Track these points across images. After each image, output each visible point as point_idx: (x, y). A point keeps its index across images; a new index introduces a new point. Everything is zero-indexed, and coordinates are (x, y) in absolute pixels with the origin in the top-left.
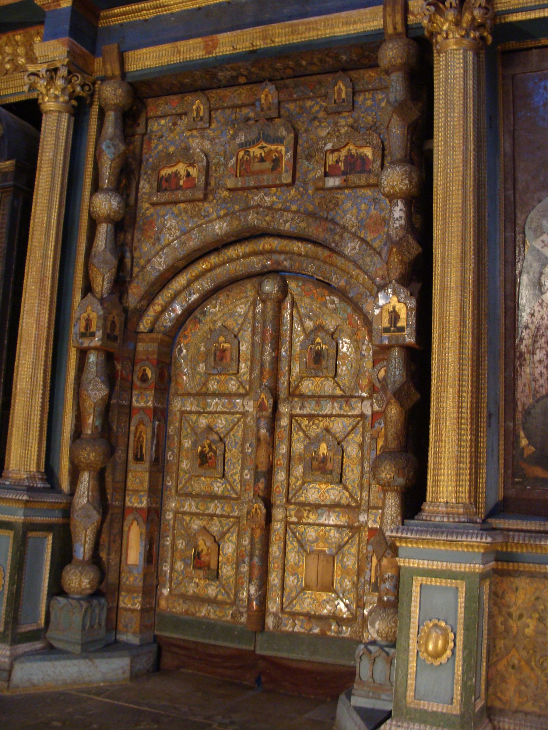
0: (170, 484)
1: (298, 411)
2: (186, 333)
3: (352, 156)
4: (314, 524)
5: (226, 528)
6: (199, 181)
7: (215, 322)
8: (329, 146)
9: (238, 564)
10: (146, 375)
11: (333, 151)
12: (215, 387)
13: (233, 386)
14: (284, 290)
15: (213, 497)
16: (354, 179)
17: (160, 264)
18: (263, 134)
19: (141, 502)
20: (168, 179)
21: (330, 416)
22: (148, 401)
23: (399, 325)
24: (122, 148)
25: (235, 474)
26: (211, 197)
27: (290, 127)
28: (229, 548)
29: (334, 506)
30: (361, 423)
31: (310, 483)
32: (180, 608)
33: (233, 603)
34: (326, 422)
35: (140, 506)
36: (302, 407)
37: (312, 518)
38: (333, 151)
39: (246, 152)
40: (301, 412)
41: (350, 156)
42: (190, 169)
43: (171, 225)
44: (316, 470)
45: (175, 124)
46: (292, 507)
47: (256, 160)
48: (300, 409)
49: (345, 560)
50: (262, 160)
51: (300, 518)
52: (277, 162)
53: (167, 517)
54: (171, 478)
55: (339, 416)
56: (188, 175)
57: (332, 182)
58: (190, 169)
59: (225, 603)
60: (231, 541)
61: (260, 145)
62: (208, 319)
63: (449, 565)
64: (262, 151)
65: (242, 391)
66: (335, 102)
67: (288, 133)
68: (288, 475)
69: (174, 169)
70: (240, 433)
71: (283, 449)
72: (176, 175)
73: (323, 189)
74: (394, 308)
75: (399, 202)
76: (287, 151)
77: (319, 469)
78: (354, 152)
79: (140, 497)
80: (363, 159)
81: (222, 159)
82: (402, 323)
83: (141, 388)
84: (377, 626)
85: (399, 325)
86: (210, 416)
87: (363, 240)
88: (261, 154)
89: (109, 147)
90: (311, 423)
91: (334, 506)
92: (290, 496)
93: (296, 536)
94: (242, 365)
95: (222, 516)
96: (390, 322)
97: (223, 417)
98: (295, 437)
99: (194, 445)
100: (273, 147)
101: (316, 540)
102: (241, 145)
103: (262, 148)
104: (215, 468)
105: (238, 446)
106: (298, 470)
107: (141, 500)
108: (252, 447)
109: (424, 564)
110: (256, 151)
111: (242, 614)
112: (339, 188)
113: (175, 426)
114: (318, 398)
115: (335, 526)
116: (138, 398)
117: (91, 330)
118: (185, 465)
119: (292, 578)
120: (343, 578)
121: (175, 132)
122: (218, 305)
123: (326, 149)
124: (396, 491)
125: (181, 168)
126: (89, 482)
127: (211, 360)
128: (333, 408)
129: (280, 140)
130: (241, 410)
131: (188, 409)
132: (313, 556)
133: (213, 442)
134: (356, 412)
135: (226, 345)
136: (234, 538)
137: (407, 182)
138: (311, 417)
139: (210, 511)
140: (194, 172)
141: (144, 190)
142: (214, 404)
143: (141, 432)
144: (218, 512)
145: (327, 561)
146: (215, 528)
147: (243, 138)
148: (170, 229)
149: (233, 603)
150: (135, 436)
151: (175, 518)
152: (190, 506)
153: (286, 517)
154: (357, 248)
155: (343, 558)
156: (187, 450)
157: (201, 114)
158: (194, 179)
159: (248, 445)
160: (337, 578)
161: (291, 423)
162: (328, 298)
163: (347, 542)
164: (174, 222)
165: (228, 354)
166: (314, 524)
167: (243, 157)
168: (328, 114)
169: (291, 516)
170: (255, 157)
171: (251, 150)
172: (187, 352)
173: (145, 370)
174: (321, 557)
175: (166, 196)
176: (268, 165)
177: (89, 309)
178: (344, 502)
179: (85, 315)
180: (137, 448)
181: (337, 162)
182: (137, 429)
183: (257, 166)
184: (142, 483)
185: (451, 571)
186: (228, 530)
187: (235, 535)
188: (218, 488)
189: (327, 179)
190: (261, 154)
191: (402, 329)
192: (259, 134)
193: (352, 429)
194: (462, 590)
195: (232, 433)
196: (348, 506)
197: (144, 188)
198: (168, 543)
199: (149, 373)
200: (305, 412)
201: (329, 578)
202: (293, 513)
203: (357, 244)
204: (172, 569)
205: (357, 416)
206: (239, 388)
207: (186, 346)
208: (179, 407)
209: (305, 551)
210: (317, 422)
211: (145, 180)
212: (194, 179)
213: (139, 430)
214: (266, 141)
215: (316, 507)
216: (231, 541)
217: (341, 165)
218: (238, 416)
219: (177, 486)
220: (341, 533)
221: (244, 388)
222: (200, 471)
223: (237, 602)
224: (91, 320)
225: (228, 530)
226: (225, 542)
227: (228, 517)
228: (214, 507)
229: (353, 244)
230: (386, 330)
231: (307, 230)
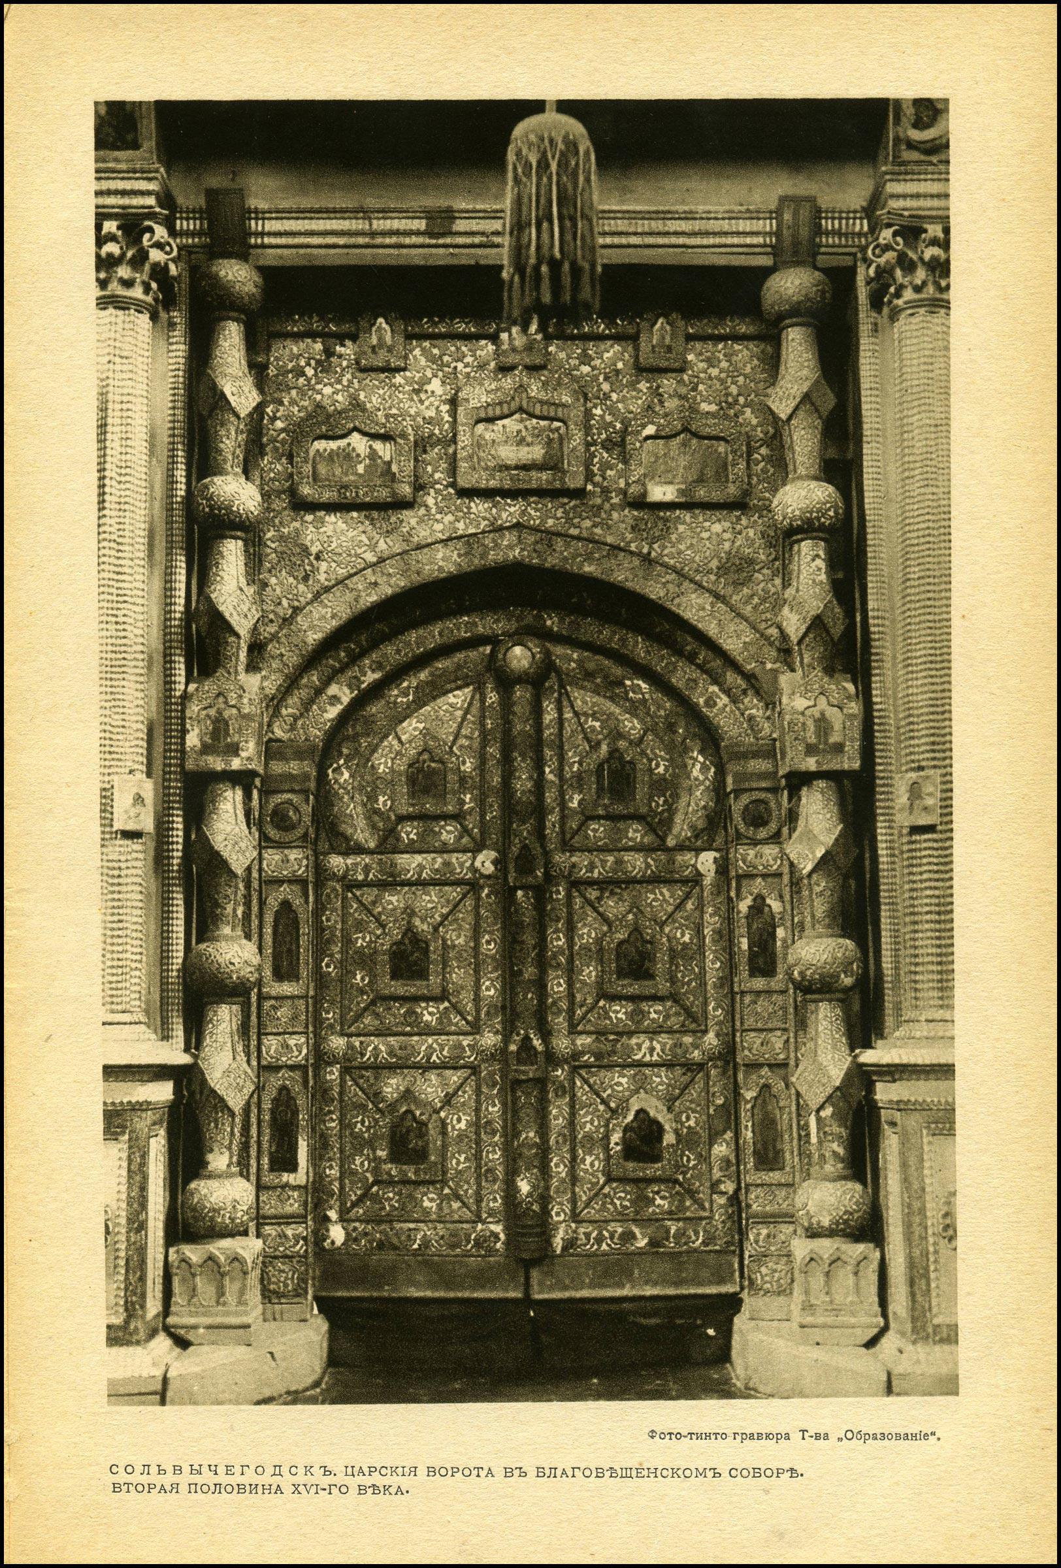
56: (373, 455)
74: (822, 714)
96: (818, 736)
154: (708, 607)
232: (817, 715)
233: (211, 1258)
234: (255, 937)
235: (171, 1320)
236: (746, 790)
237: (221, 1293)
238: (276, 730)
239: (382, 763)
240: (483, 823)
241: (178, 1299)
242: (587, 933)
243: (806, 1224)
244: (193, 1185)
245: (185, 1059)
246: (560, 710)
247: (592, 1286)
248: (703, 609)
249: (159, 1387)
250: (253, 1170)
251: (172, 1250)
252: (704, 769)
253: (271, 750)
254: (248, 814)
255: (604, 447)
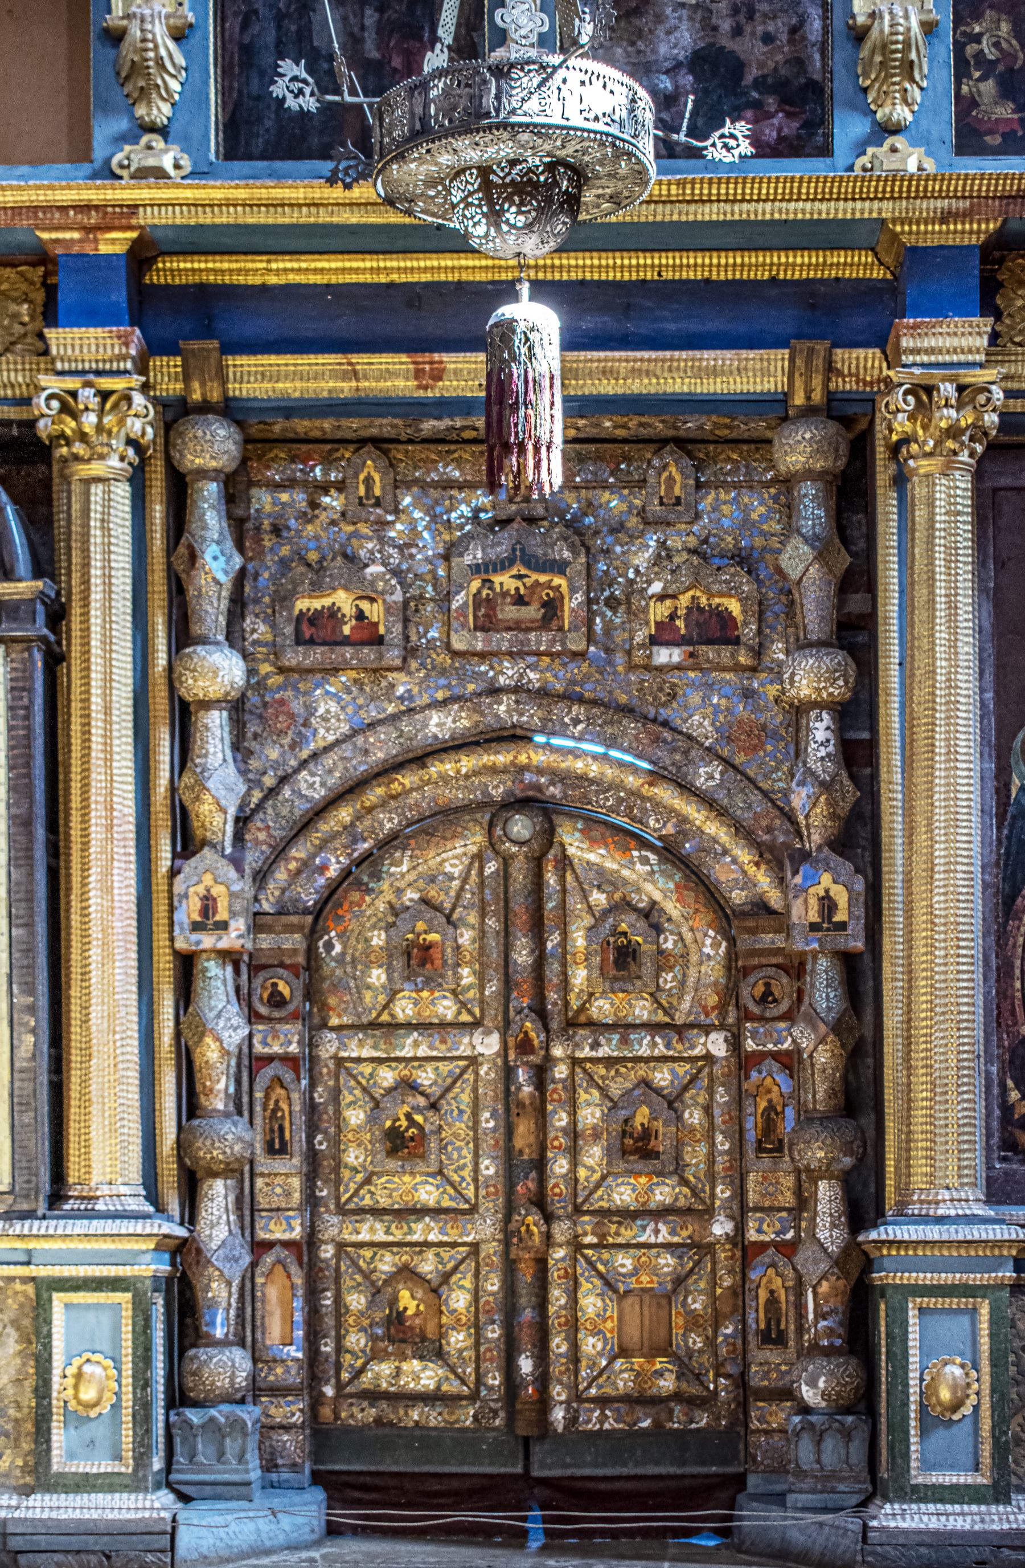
0: (324, 1193)
1: (586, 1052)
2: (340, 912)
3: (701, 610)
4: (627, 1246)
5: (450, 1266)
6: (388, 630)
7: (399, 892)
8: (656, 587)
9: (477, 1328)
10: (281, 994)
11: (662, 597)
12: (409, 1012)
13: (446, 1008)
14: (548, 835)
15: (420, 1212)
16: (709, 652)
17: (311, 786)
18: (522, 550)
19: (292, 1229)
20: (314, 619)
21: (647, 1060)
22: (290, 1043)
23: (836, 919)
24: (238, 561)
25: (462, 1168)
26: (414, 665)
27: (578, 543)
28: (460, 1300)
29: (662, 1213)
30: (707, 1070)
31: (617, 1175)
32: (364, 1414)
33: (473, 1397)
34: (642, 1070)
35: (286, 1236)
36: (595, 1045)
37: (627, 1235)
38: (662, 597)
39: (484, 581)
40: (594, 1054)
41: (695, 608)
42: (365, 605)
43: (328, 711)
44: (631, 1153)
45: (314, 505)
46: (586, 1218)
47: (508, 600)
48: (592, 1048)
49: (690, 1300)
50: (520, 600)
51: (603, 1236)
52: (552, 607)
53: (323, 1255)
54: (326, 1181)
55: (664, 1059)
56: (360, 616)
57: (664, 656)
58: (365, 605)
59: (459, 1397)
60: (462, 1287)
61: (514, 572)
62: (385, 885)
63: (965, 1276)
64: (519, 584)
65: (465, 1018)
66: (661, 504)
67: (575, 553)
68: (575, 1164)
69: (327, 602)
70: (466, 1098)
71: (561, 1119)
72: (333, 614)
73: (648, 668)
74: (827, 891)
75: (825, 715)
76: (573, 590)
77: (637, 1151)
78: (704, 601)
79: (288, 1219)
80: (724, 618)
81: (430, 588)
82: (840, 916)
83: (270, 1019)
84: (821, 1384)
85: (836, 919)
86: (402, 1066)
87: (727, 762)
88: (517, 589)
89: (215, 558)
90: (613, 1073)
91: (662, 1213)
92: (580, 1200)
93: (595, 1269)
94: (465, 971)
95: (441, 1244)
96: (821, 913)
97: (429, 1067)
98: (583, 1096)
99: (372, 1119)
100: (543, 578)
101: (635, 1272)
102: (476, 569)
103: (520, 577)
104: (423, 1157)
105: (465, 1117)
106: (594, 1155)
107: (289, 1224)
108: (496, 1120)
109: (927, 1278)
110: (505, 581)
111: (495, 1412)
112: (678, 667)
113: (326, 1086)
114: (624, 1028)
115: (667, 1246)
116: (265, 1037)
117: (218, 918)
118: (353, 1156)
119: (591, 1340)
120: (687, 1330)
121: (318, 521)
122: (406, 859)
123: (650, 592)
124: (837, 1178)
125: (343, 600)
126: (226, 1197)
127: (398, 964)
128: (654, 1045)
129: (560, 567)
130: (468, 1053)
131: (354, 1055)
132: (630, 1300)
133: (417, 1109)
134: (698, 1051)
135: (434, 937)
136: (468, 1283)
137: (841, 683)
138: (609, 1062)
139: (416, 1237)
140: (374, 611)
141: (255, 636)
142: (409, 1046)
143: (277, 1102)
144: (432, 1237)
145: (659, 1304)
146: (428, 1266)
147: (479, 555)
148: (326, 720)
149: (473, 1397)
150: (265, 1109)
151: (337, 1256)
152: (371, 1230)
153: (576, 1237)
154: (717, 776)
155: (686, 1297)
156: (357, 1130)
157: (377, 492)
158: (376, 625)
159: (487, 1115)
160: (678, 1332)
161: (572, 1073)
162: (635, 853)
163: (692, 1270)
164: (333, 707)
165: (435, 953)
166: (627, 1246)
167: (479, 591)
168: (647, 523)
169: (585, 1234)
170: (505, 594)
171: (497, 579)
172: (345, 947)
173: (275, 985)
174: (646, 1298)
175: (317, 655)
176: (532, 612)
177: (208, 879)
178: (682, 1202)
179: (201, 889)
180: (272, 1131)
181: (673, 617)
182: (267, 1097)
183: (509, 612)
184: (288, 1194)
185: (966, 1286)
186: (455, 1269)
187: (469, 1276)
188: (428, 1194)
189: (655, 649)
190: (517, 589)
191: (842, 926)
192: (514, 550)
193: (691, 1082)
194: (985, 1311)
195: (451, 1095)
196: (689, 1211)
197: (254, 631)
198: (328, 1302)
199: (283, 988)
200: (601, 1053)
201: (663, 1333)
202: (588, 1228)
203: (716, 769)
204: (339, 1349)
205: (697, 1058)
206: (459, 1013)
207: (340, 936)
208: (333, 1050)
209: (615, 1291)
210: (623, 1070)
211: (257, 616)
212: (376, 625)
213: (274, 1097)
214: (528, 566)
215: (628, 1215)
216: (462, 1287)
217: (680, 623)
218: (462, 1063)
219: (338, 1198)
220: (680, 1258)
221: (470, 1012)
222: (393, 1164)
223: (483, 1393)
224: (215, 900)
225: (455, 1269)
226: (451, 1290)
227: (454, 1245)
228: (421, 1230)
229: (709, 769)
230: (814, 927)
231: (839, 811)
232: (822, 893)
233: (212, 1419)
234: (246, 1114)
235: (174, 1477)
236: (755, 968)
237: (221, 1455)
238: (264, 903)
239: (823, 963)
240: (482, 1002)
241: (180, 1458)
242: (590, 1115)
243: (575, 1004)
244: (192, 1352)
245: (182, 1232)
246: (562, 879)
247: (595, 1465)
248: (712, 778)
249: (169, 1529)
250: (249, 1339)
251: (172, 1413)
252: (715, 946)
253: (258, 923)
254: (238, 990)
255: (607, 605)
